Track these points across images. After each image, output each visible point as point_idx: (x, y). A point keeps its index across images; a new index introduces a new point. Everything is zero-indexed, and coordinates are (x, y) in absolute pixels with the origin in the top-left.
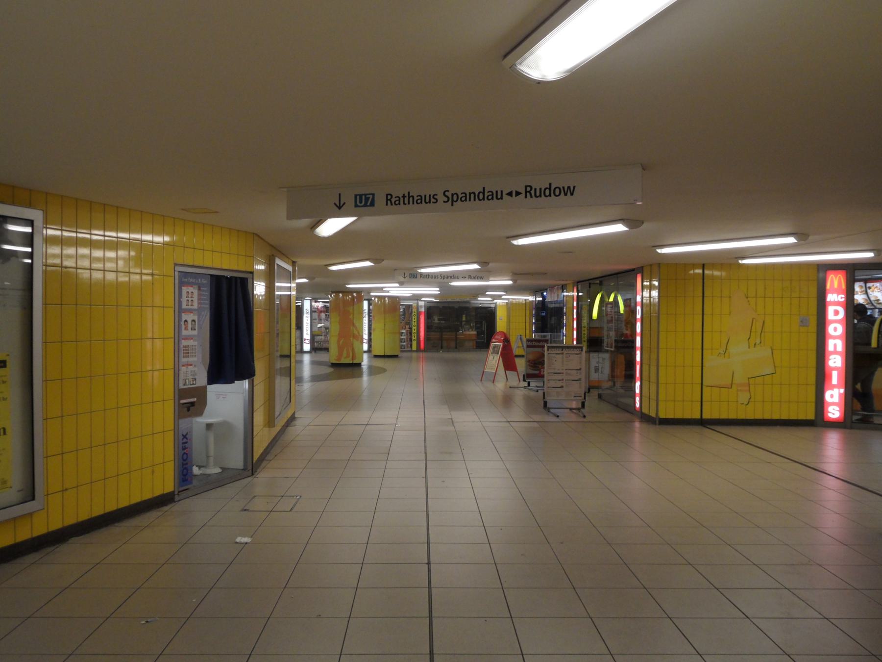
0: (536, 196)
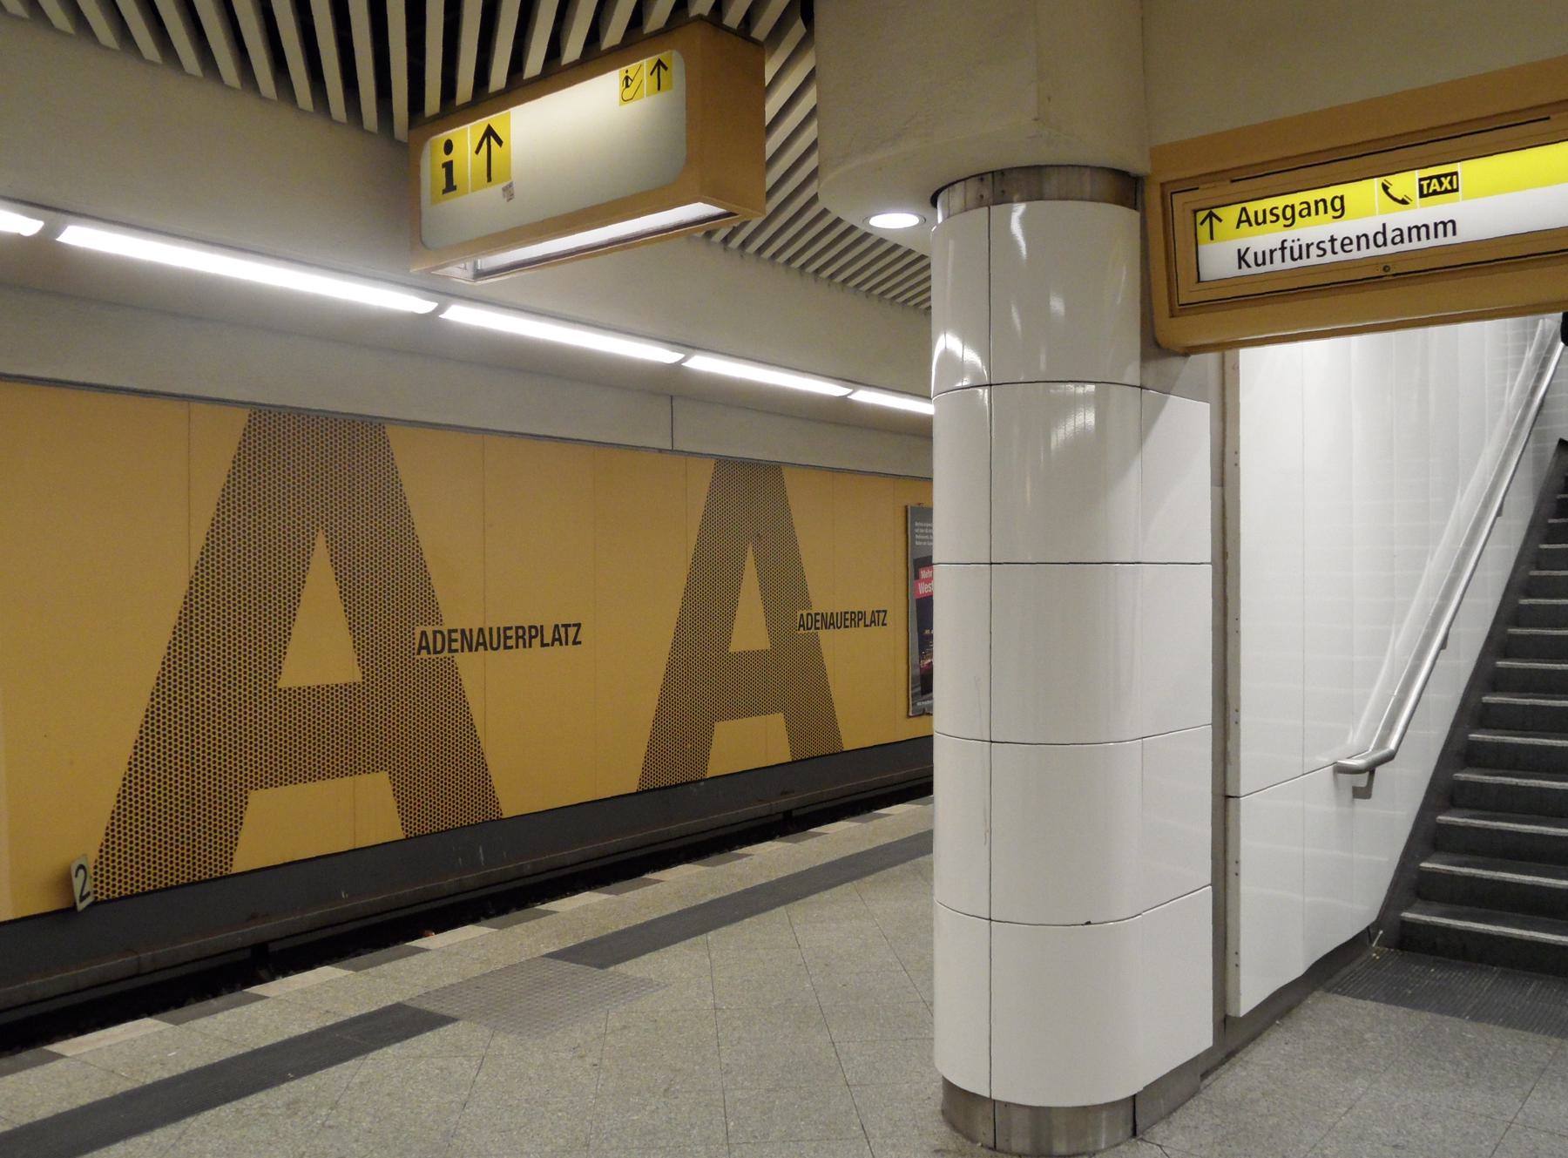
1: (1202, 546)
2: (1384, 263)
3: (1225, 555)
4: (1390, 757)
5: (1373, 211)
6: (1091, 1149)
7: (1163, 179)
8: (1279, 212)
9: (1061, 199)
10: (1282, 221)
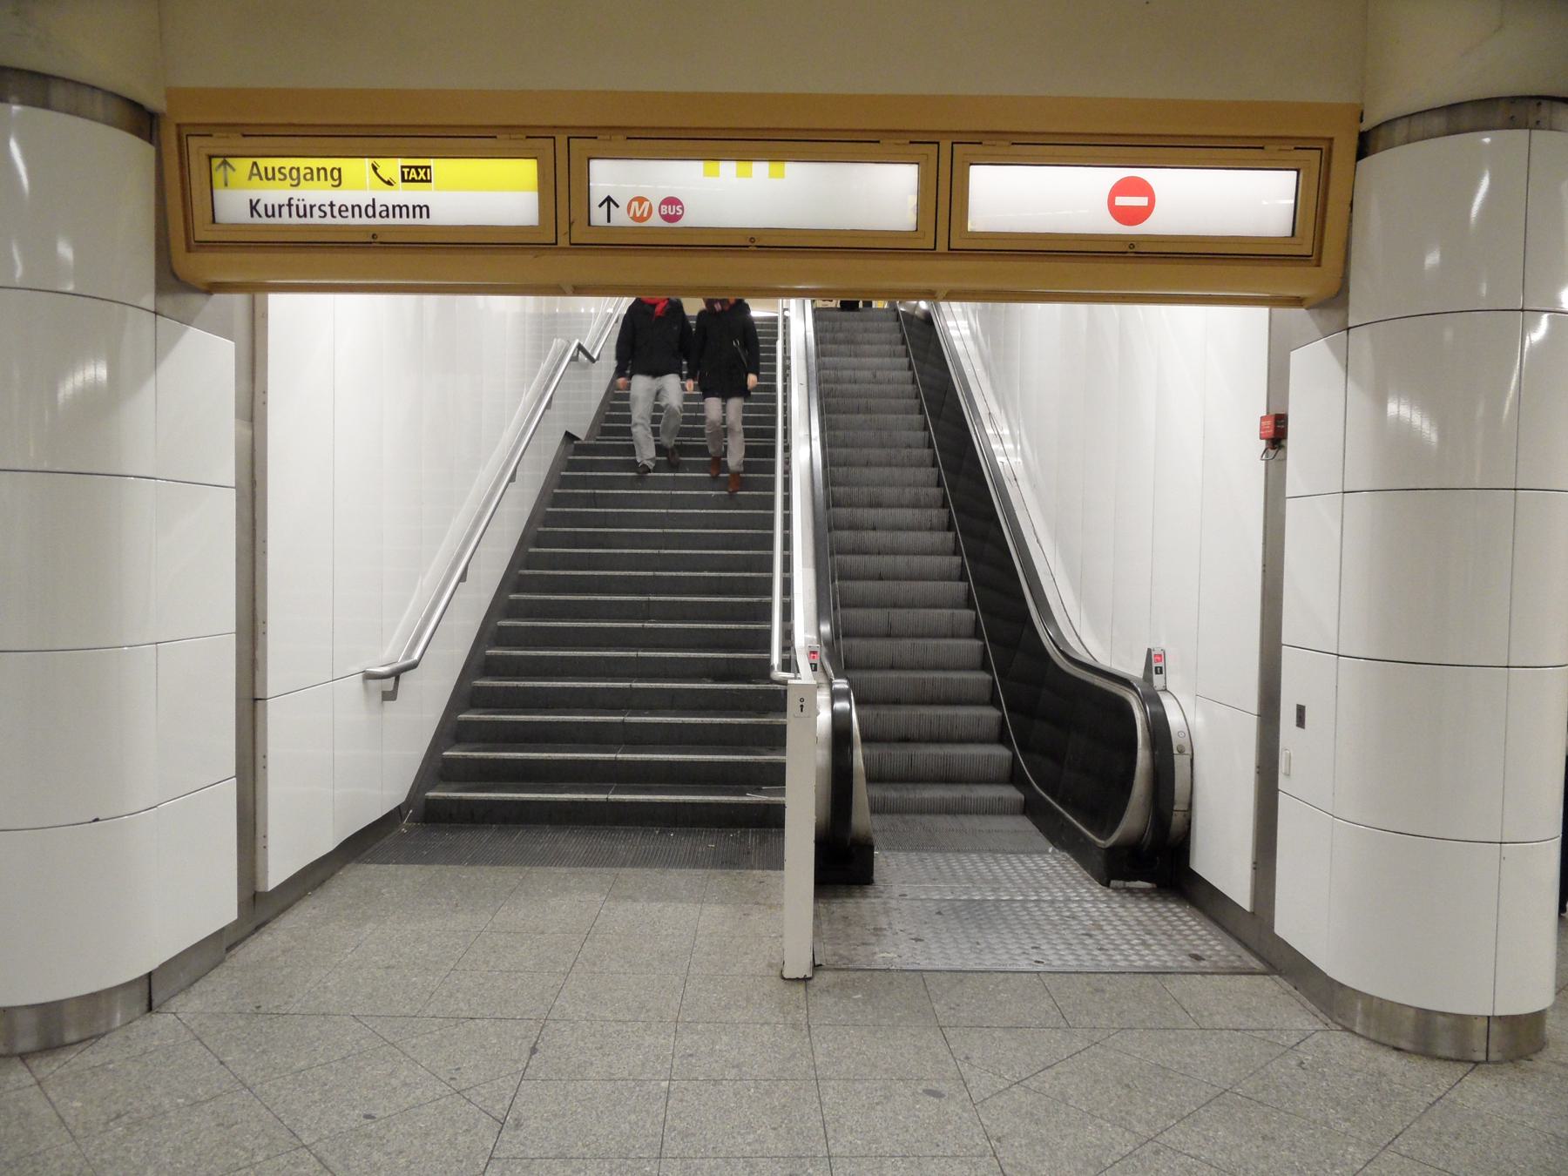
1: (226, 471)
2: (374, 232)
3: (253, 483)
4: (414, 666)
5: (360, 185)
6: (103, 1030)
7: (185, 119)
8: (286, 171)
9: (68, 112)
10: (288, 180)
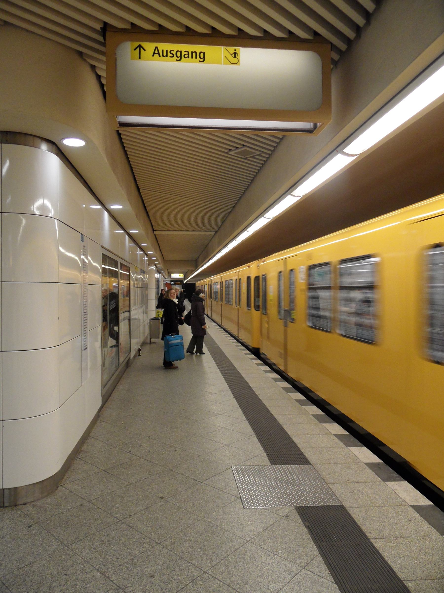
0: (163, 56)
8: (174, 53)
